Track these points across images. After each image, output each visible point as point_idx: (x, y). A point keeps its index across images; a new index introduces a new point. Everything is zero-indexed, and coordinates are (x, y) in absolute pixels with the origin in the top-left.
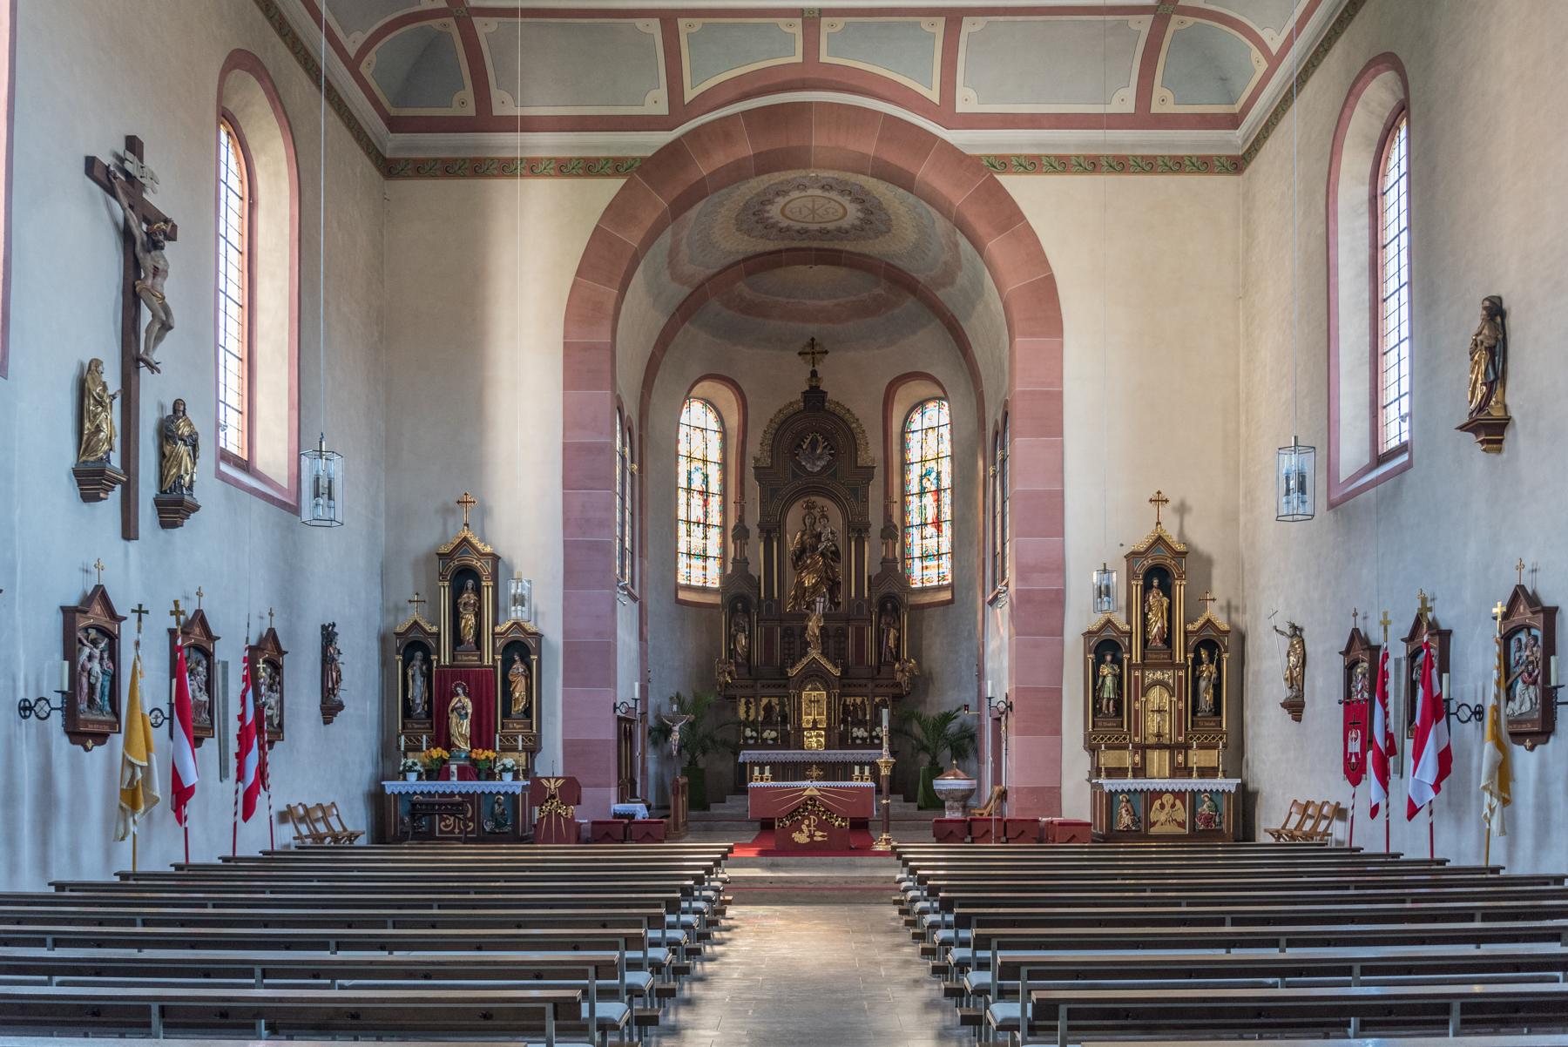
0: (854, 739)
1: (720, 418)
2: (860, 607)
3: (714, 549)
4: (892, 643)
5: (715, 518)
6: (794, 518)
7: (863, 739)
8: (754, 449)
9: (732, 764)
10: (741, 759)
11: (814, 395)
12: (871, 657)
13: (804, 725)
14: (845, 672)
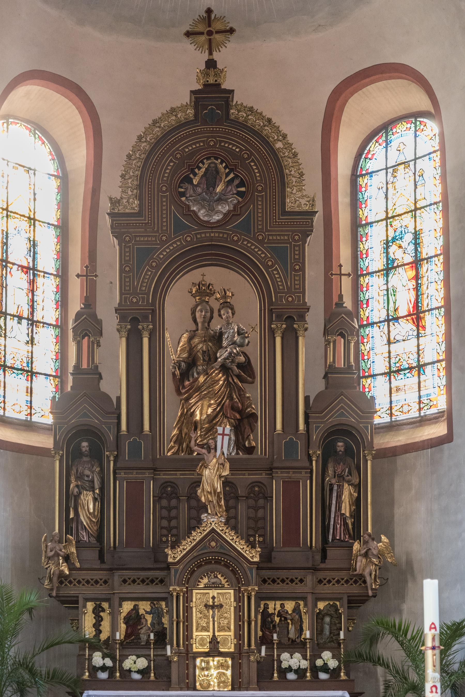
0: (283, 672)
1: (59, 156)
2: (291, 446)
3: (46, 361)
4: (346, 509)
5: (48, 311)
6: (177, 305)
7: (300, 672)
8: (112, 187)
11: (212, 99)
12: (311, 534)
13: (196, 648)
14: (267, 557)
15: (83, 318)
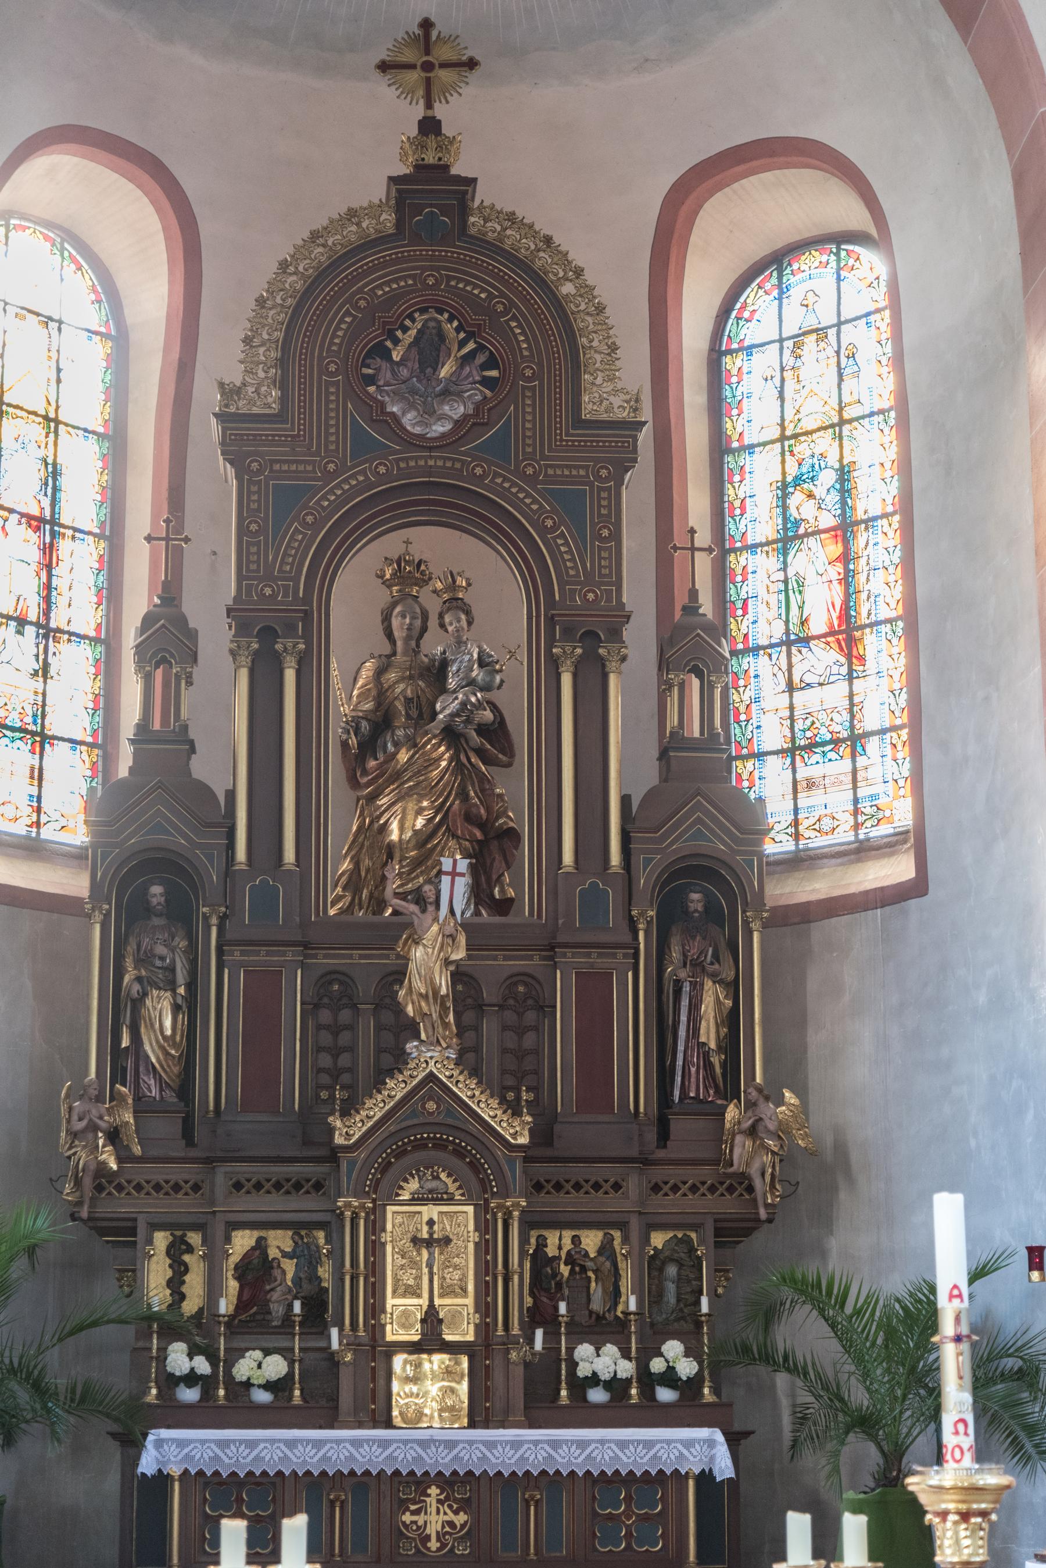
0: (580, 1386)
2: (593, 900)
3: (72, 712)
4: (709, 1034)
5: (79, 609)
6: (355, 600)
7: (616, 1386)
8: (223, 359)
9: (112, 1482)
10: (147, 1465)
11: (432, 195)
13: (393, 1333)
15: (158, 625)
